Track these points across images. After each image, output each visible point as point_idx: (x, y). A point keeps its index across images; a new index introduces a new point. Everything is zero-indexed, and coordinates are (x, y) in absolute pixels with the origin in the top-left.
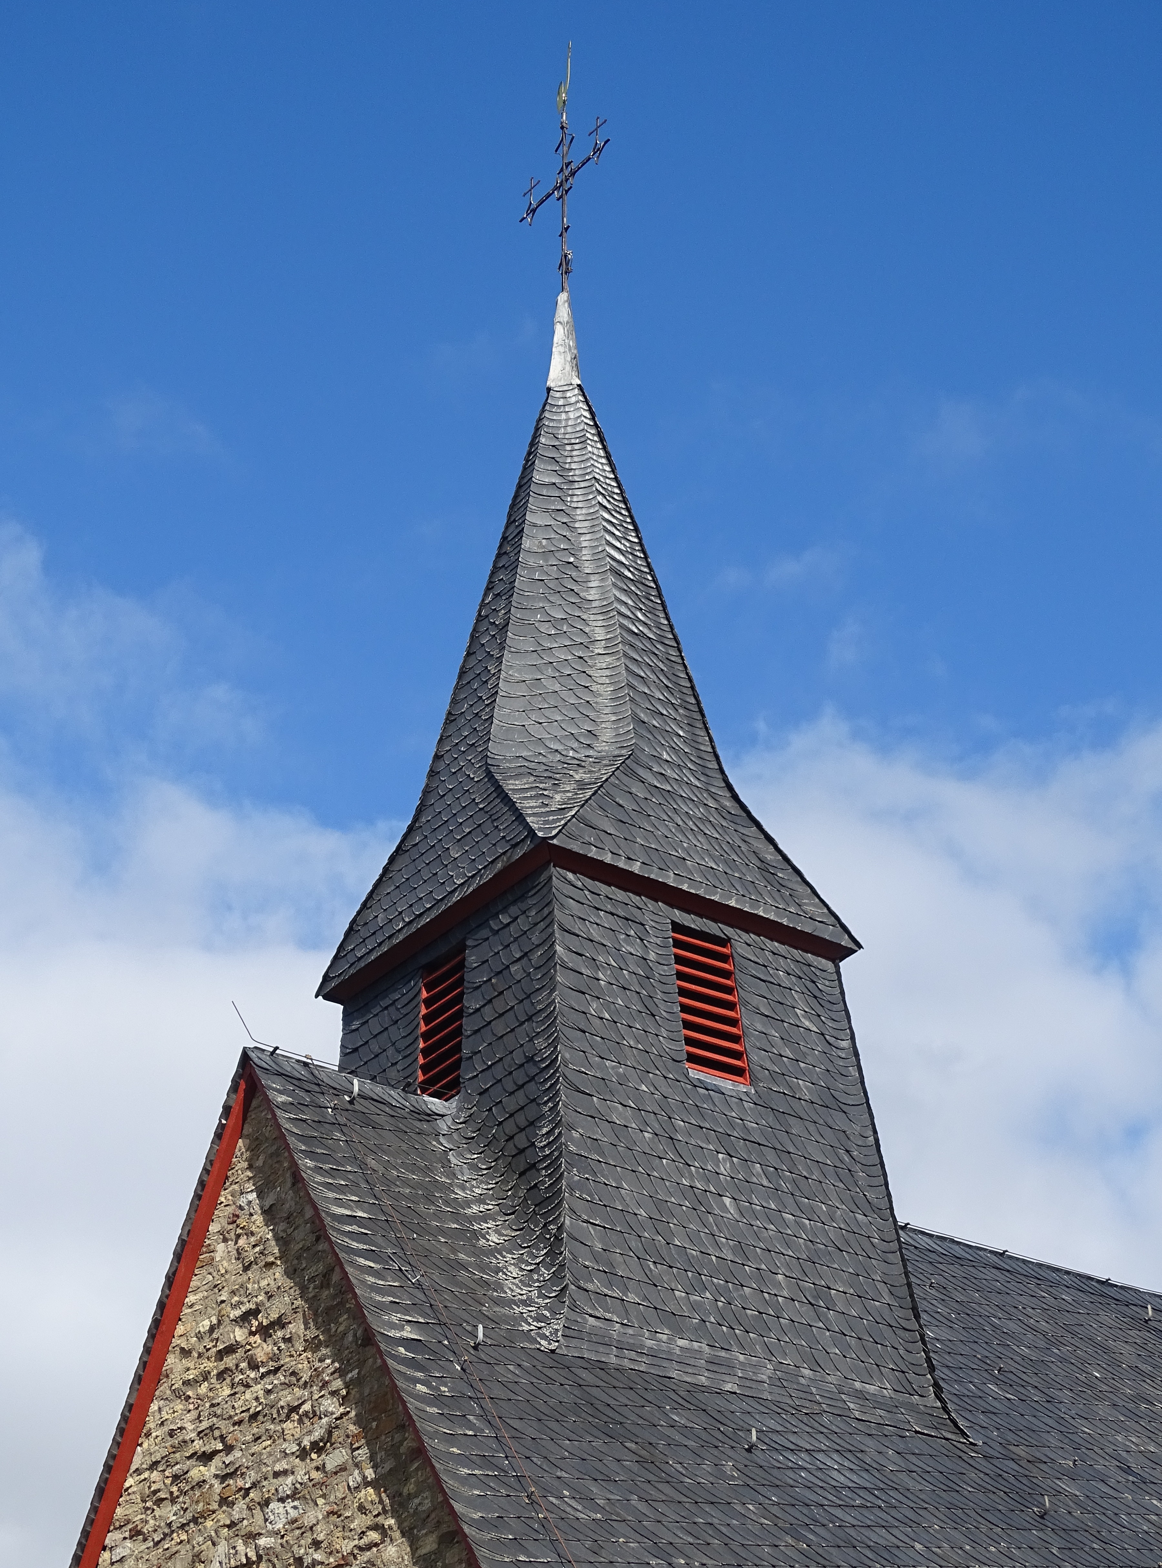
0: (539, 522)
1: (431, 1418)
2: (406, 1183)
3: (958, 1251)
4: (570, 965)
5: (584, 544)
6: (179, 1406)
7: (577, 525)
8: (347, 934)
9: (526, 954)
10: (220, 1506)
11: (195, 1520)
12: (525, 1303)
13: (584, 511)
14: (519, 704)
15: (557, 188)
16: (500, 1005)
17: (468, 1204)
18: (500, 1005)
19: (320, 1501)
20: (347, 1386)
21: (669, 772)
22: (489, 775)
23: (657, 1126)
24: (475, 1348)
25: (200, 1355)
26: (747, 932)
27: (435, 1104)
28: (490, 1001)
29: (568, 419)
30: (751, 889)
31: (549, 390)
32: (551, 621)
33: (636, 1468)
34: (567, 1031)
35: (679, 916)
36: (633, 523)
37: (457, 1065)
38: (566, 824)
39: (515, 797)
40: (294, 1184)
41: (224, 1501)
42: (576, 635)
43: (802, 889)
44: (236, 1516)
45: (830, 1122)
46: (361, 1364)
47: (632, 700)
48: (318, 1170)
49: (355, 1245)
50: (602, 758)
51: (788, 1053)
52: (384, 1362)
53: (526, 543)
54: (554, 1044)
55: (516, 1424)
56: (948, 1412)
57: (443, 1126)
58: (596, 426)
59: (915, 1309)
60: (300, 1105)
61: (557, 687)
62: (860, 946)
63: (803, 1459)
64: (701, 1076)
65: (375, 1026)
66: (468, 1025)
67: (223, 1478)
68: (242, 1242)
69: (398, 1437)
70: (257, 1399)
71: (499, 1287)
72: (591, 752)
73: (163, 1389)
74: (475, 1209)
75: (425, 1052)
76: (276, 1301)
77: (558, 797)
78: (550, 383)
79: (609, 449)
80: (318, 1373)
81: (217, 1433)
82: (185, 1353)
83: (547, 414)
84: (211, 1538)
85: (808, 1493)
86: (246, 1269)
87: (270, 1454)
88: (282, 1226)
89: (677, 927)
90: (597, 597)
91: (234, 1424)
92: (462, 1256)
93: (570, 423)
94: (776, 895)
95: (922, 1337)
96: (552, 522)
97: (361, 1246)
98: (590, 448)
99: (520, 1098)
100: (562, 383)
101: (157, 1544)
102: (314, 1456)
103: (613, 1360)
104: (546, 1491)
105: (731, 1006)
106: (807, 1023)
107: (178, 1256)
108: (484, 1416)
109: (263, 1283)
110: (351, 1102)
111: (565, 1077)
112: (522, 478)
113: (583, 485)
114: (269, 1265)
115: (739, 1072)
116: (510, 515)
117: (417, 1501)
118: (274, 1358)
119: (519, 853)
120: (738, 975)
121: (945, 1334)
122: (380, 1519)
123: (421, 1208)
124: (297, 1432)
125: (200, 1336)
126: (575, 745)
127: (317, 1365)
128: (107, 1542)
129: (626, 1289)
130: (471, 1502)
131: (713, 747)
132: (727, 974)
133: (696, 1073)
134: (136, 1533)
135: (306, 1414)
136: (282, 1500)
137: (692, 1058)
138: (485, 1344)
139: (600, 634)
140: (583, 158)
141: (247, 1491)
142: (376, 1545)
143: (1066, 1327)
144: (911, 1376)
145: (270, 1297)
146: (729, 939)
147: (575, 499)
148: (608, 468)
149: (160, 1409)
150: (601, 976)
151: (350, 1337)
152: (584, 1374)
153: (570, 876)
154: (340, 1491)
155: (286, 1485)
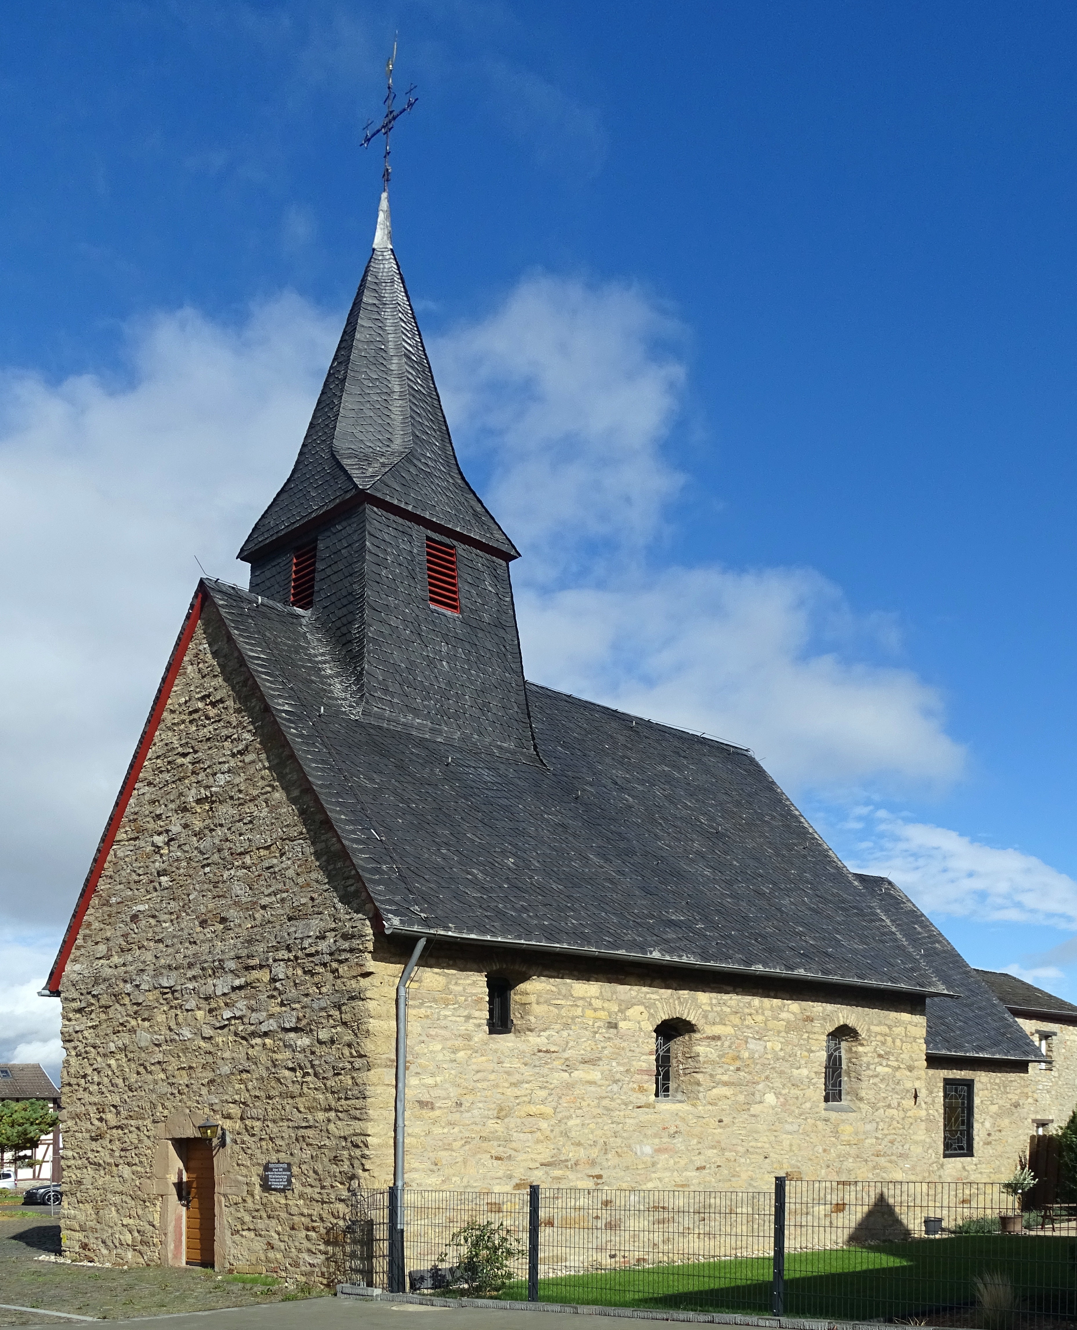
0: (365, 325)
1: (297, 743)
2: (285, 644)
3: (550, 693)
4: (373, 551)
5: (390, 339)
6: (170, 734)
7: (387, 328)
8: (253, 530)
9: (350, 545)
10: (192, 774)
11: (180, 780)
12: (343, 699)
13: (391, 321)
14: (351, 421)
15: (384, 127)
16: (335, 568)
17: (316, 656)
18: (335, 568)
19: (242, 774)
20: (255, 728)
21: (430, 463)
22: (333, 456)
23: (412, 628)
24: (320, 716)
25: (180, 713)
26: (464, 544)
27: (300, 611)
28: (330, 566)
29: (384, 268)
30: (468, 523)
31: (374, 250)
32: (370, 379)
33: (394, 769)
34: (370, 582)
35: (430, 533)
36: (418, 331)
37: (312, 594)
38: (373, 484)
39: (347, 468)
40: (228, 642)
41: (193, 773)
42: (383, 387)
43: (493, 526)
44: (200, 779)
45: (497, 633)
46: (262, 720)
47: (412, 424)
48: (240, 635)
49: (260, 669)
50: (395, 452)
51: (479, 601)
52: (275, 720)
53: (358, 336)
54: (363, 587)
55: (338, 748)
56: (539, 757)
57: (304, 621)
58: (400, 274)
59: (529, 715)
60: (231, 606)
61: (372, 414)
62: (520, 555)
63: (471, 770)
64: (436, 608)
65: (268, 574)
66: (318, 576)
67: (193, 764)
68: (200, 665)
69: (281, 750)
70: (210, 732)
71: (331, 692)
72: (389, 449)
73: (162, 726)
74: (320, 658)
75: (294, 588)
76: (219, 692)
77: (370, 470)
78: (375, 246)
79: (407, 288)
80: (241, 722)
81: (190, 745)
82: (173, 712)
83: (372, 264)
84: (187, 787)
85: (474, 784)
86: (203, 677)
87: (217, 755)
88: (222, 659)
89: (428, 538)
90: (396, 368)
91: (199, 742)
92: (313, 678)
93: (386, 270)
94: (480, 527)
95: (531, 726)
96: (373, 326)
97: (263, 670)
98: (396, 286)
99: (344, 611)
100: (382, 247)
101: (160, 788)
102: (239, 756)
103: (385, 725)
104: (352, 775)
105: (453, 577)
106: (490, 588)
107: (168, 670)
108: (323, 744)
109: (212, 684)
110: (257, 607)
111: (368, 603)
112: (356, 299)
113: (391, 306)
114: (215, 676)
115: (455, 607)
116: (348, 320)
117: (290, 776)
118: (218, 715)
119: (348, 496)
120: (458, 564)
121: (540, 726)
122: (272, 783)
123: (293, 656)
124: (231, 746)
125: (180, 705)
126: (381, 445)
127: (240, 719)
128: (136, 786)
129: (393, 697)
130: (316, 777)
131: (454, 453)
132: (452, 563)
133: (433, 606)
134: (149, 784)
135: (235, 739)
136: (223, 773)
137: (432, 600)
138: (324, 715)
139: (397, 388)
140: (400, 109)
141: (205, 769)
142: (270, 792)
143: (596, 728)
144: (524, 741)
145: (216, 689)
146: (455, 547)
147: (386, 314)
148: (405, 298)
149: (160, 735)
150: (389, 558)
151: (258, 708)
152: (371, 730)
153: (375, 509)
154: (252, 771)
155: (225, 767)
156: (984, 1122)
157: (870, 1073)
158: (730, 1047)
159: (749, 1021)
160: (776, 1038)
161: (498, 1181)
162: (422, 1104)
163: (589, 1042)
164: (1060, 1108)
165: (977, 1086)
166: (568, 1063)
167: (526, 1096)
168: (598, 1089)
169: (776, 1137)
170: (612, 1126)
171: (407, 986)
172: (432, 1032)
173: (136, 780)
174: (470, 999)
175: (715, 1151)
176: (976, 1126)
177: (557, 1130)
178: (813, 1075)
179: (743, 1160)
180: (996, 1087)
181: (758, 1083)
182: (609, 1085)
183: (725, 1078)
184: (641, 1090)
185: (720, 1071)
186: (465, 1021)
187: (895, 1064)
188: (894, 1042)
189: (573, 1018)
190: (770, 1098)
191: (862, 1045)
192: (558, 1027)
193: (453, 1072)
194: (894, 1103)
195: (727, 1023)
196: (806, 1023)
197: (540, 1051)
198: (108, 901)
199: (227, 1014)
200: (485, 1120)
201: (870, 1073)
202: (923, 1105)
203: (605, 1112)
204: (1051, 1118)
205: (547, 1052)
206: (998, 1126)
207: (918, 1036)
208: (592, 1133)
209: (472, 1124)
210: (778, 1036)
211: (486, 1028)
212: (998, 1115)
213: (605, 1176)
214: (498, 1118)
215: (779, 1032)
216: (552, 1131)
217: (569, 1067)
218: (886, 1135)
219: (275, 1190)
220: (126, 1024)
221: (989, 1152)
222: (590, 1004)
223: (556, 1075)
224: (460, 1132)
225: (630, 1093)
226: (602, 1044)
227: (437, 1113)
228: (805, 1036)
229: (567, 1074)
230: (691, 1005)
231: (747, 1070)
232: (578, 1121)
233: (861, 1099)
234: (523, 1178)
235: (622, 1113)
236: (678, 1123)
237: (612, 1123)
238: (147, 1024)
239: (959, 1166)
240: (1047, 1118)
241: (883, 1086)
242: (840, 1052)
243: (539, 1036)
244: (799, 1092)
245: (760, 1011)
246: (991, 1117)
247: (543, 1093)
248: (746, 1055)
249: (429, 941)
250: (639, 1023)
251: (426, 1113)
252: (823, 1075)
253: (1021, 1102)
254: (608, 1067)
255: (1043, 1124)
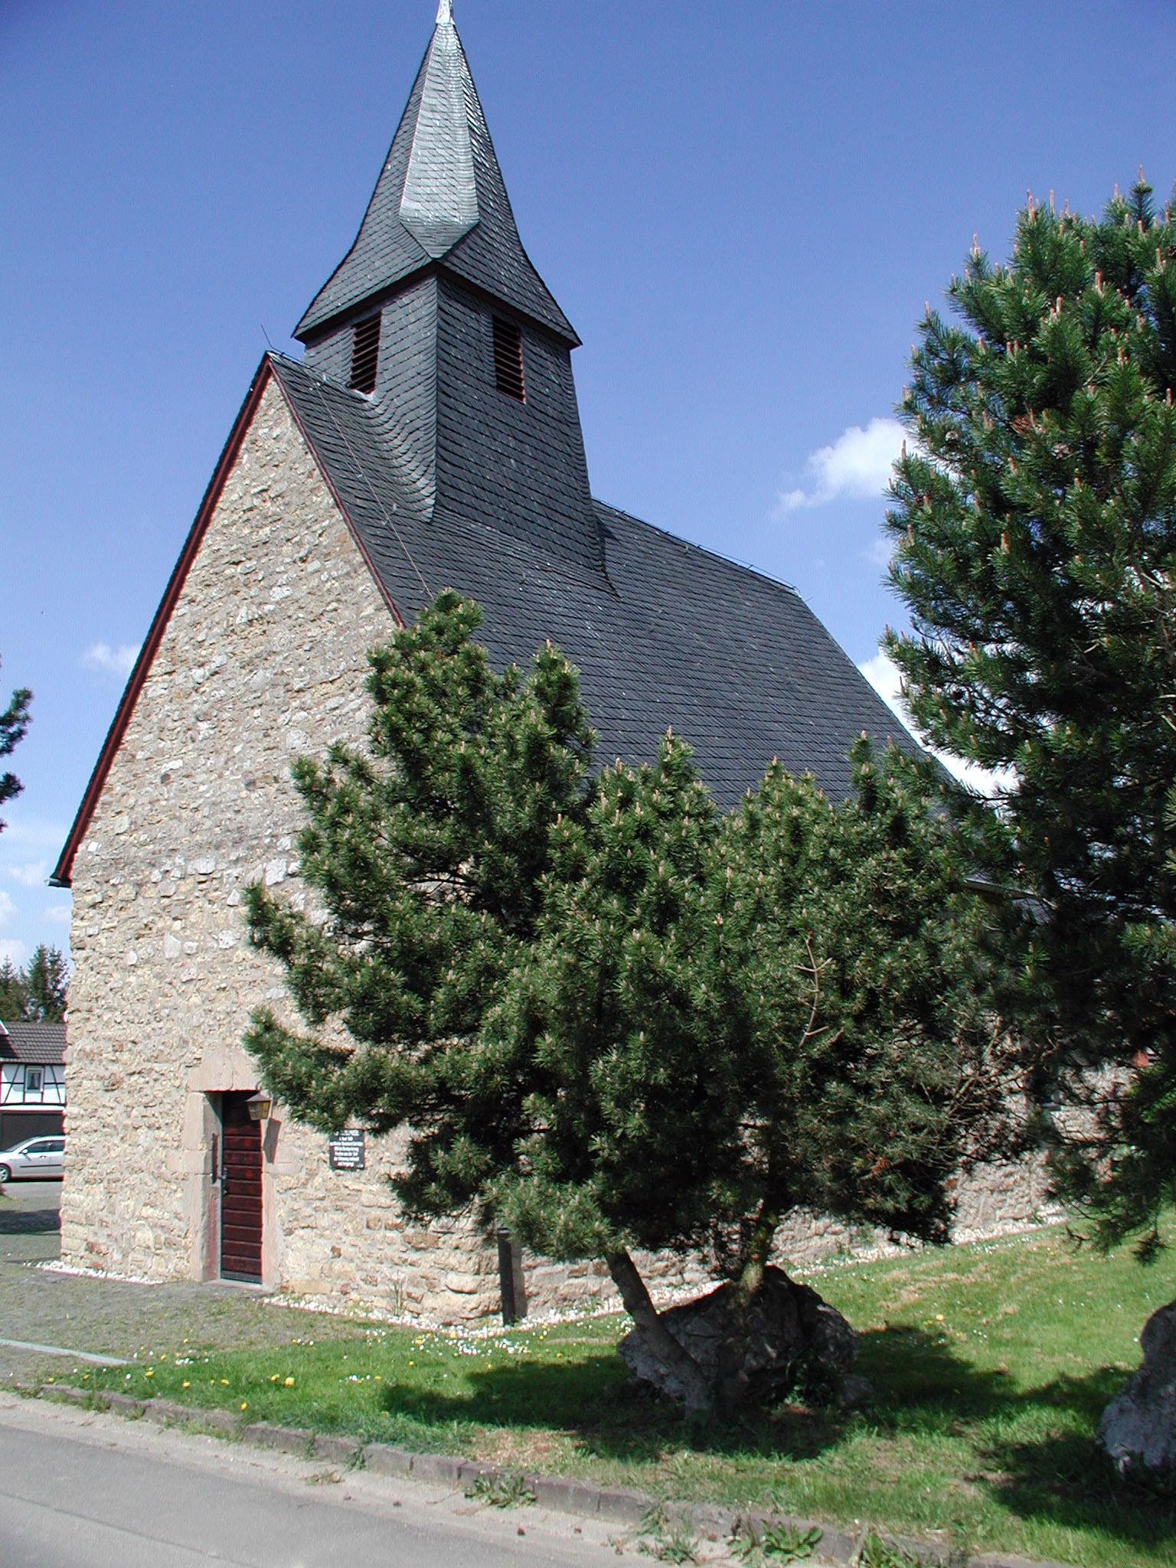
66: (381, 355)
78: (438, 21)
109: (272, 476)
173: (175, 599)
198: (134, 757)
219: (342, 1168)
220: (151, 925)
238: (178, 925)
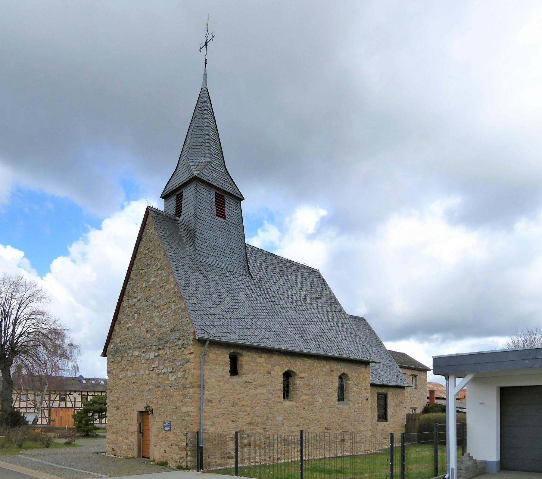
3: (255, 249)
66: (183, 205)
133: (217, 218)
137: (217, 215)
156: (391, 409)
157: (352, 391)
158: (307, 381)
159: (313, 372)
160: (322, 378)
161: (233, 429)
162: (209, 401)
163: (262, 379)
164: (420, 403)
165: (388, 396)
166: (255, 386)
167: (242, 398)
168: (265, 396)
169: (322, 414)
170: (269, 410)
171: (204, 358)
172: (212, 374)
174: (224, 363)
175: (303, 419)
176: (388, 410)
177: (252, 411)
178: (334, 392)
179: (311, 423)
180: (395, 396)
181: (316, 394)
182: (268, 395)
183: (305, 392)
184: (279, 396)
185: (304, 390)
186: (223, 371)
187: (360, 387)
188: (360, 379)
189: (257, 370)
190: (320, 400)
191: (350, 380)
192: (251, 373)
193: (219, 389)
194: (360, 402)
195: (306, 372)
196: (331, 372)
197: (246, 382)
199: (153, 366)
200: (229, 407)
201: (352, 391)
202: (370, 403)
203: (267, 405)
204: (417, 407)
205: (248, 382)
206: (396, 410)
207: (368, 377)
208: (263, 412)
209: (225, 408)
210: (322, 377)
211: (229, 373)
212: (396, 406)
213: (267, 428)
214: (233, 406)
215: (323, 376)
216: (250, 411)
217: (255, 388)
218: (357, 414)
221: (392, 420)
222: (262, 365)
223: (251, 391)
224: (221, 411)
225: (275, 398)
226: (266, 380)
227: (214, 404)
228: (331, 377)
229: (255, 391)
230: (294, 366)
231: (312, 390)
232: (258, 408)
233: (349, 400)
234: (241, 428)
235: (272, 405)
236: (291, 409)
237: (269, 409)
239: (383, 425)
240: (415, 407)
241: (356, 395)
242: (343, 383)
243: (246, 376)
244: (329, 398)
245: (316, 368)
246: (393, 407)
247: (247, 398)
248: (312, 384)
249: (210, 342)
250: (278, 372)
251: (210, 404)
252: (337, 391)
253: (403, 401)
254: (268, 388)
255: (415, 409)
